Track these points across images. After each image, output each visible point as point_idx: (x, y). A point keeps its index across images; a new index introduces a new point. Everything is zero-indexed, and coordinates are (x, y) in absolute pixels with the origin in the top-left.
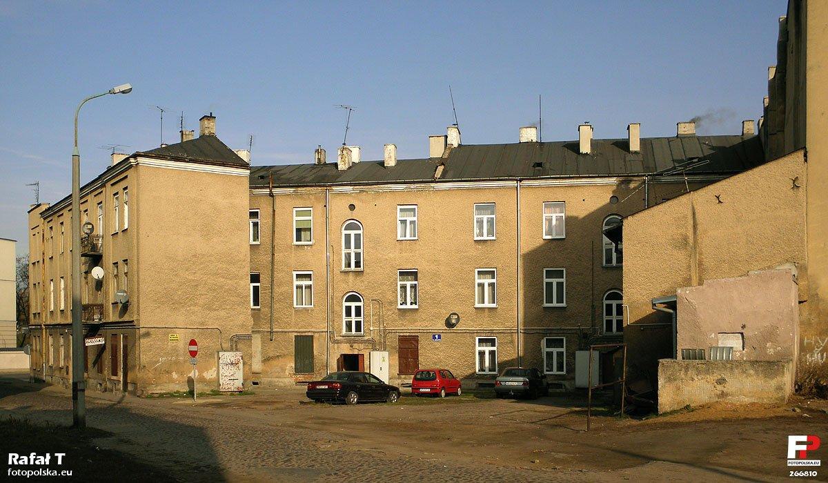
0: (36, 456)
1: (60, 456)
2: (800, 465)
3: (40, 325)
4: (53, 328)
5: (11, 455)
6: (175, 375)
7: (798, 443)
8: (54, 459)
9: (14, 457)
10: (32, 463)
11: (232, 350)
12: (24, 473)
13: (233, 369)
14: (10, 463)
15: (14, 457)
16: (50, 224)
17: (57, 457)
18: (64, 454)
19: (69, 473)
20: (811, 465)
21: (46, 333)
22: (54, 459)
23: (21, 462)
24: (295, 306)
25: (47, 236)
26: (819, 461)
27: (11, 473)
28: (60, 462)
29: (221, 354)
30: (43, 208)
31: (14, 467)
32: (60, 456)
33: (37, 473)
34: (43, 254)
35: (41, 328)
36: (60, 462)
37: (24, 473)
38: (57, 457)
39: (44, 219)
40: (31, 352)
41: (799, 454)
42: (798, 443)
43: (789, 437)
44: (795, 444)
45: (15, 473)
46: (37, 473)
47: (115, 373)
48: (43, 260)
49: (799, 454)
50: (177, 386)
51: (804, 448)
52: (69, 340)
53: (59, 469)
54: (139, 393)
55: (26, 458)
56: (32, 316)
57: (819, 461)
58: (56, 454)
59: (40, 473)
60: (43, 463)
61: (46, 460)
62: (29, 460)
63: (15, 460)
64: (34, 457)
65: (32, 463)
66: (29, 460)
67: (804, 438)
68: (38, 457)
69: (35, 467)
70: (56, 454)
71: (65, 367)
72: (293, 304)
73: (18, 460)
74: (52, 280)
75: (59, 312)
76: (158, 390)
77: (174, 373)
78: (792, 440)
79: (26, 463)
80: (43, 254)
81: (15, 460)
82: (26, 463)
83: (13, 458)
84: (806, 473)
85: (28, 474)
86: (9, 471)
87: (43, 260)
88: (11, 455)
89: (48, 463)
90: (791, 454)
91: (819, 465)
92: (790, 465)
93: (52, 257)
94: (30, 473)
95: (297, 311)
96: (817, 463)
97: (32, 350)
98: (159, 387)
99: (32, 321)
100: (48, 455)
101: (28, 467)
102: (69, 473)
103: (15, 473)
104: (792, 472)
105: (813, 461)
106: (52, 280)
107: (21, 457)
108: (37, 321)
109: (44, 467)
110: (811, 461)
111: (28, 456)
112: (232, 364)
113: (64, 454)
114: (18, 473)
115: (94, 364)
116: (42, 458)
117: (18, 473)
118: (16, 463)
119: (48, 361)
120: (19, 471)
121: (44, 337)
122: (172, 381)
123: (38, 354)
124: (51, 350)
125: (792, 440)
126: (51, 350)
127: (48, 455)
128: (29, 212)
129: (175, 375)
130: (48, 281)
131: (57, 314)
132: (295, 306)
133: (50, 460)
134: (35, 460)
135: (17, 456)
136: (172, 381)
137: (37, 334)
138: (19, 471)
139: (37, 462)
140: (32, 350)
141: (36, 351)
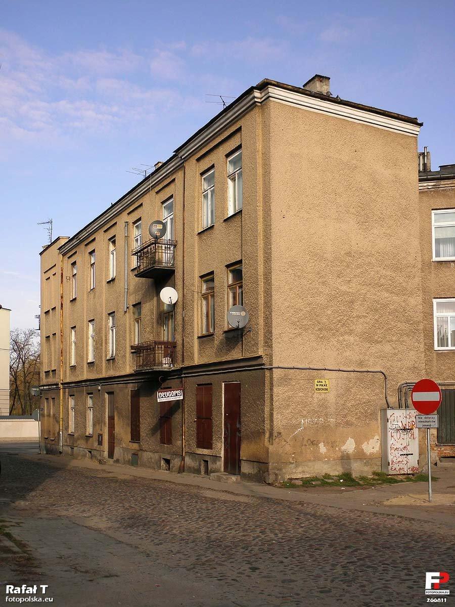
0: (27, 587)
1: (44, 587)
2: (435, 594)
3: (57, 384)
4: (76, 387)
5: (8, 587)
6: (323, 449)
7: (433, 578)
8: (39, 590)
9: (10, 588)
10: (23, 592)
11: (400, 407)
12: (18, 600)
13: (406, 437)
14: (7, 592)
15: (10, 588)
16: (72, 260)
17: (42, 588)
18: (47, 586)
19: (51, 600)
20: (443, 594)
21: (64, 393)
22: (39, 590)
23: (15, 592)
24: (436, 348)
25: (67, 273)
26: (449, 591)
27: (8, 599)
28: (44, 592)
29: (389, 412)
30: (62, 242)
31: (10, 595)
32: (44, 587)
33: (27, 600)
34: (62, 297)
35: (58, 389)
36: (44, 592)
37: (18, 600)
38: (42, 588)
39: (63, 255)
40: (41, 418)
41: (433, 585)
42: (433, 578)
43: (427, 573)
44: (431, 578)
45: (11, 600)
46: (27, 600)
47: (205, 441)
48: (62, 304)
49: (433, 585)
50: (326, 466)
51: (437, 581)
52: (104, 400)
53: (43, 596)
54: (271, 479)
55: (19, 589)
56: (43, 375)
57: (449, 591)
58: (41, 586)
59: (29, 600)
60: (31, 593)
61: (33, 590)
62: (21, 590)
63: (11, 590)
64: (25, 588)
65: (23, 592)
66: (21, 590)
67: (437, 574)
68: (28, 588)
69: (26, 595)
70: (41, 586)
71: (95, 437)
72: (433, 346)
73: (13, 590)
74: (74, 328)
75: (85, 365)
76: (299, 473)
77: (321, 445)
78: (429, 575)
79: (19, 592)
80: (62, 297)
81: (11, 590)
82: (19, 592)
83: (9, 589)
84: (439, 599)
85: (20, 600)
86: (7, 598)
87: (62, 304)
88: (8, 587)
89: (35, 592)
90: (428, 586)
91: (449, 594)
92: (427, 594)
93: (75, 299)
94: (22, 600)
95: (440, 354)
96: (447, 592)
97: (42, 415)
98: (300, 469)
99: (44, 381)
100: (35, 586)
101: (20, 595)
102: (51, 600)
103: (11, 600)
104: (429, 599)
105: (444, 591)
106: (74, 328)
107: (16, 588)
108: (51, 380)
109: (32, 595)
110: (442, 591)
111: (21, 587)
112: (405, 429)
113: (47, 586)
114: (13, 599)
115: (154, 431)
116: (31, 589)
117: (13, 599)
118: (12, 592)
119: (67, 428)
120: (14, 598)
121: (61, 398)
122: (318, 458)
123: (51, 419)
124: (72, 414)
125: (429, 575)
126: (72, 414)
127: (35, 586)
128: (41, 254)
129: (323, 449)
130: (68, 329)
131: (82, 367)
132: (436, 348)
133: (37, 590)
134: (26, 590)
135: (12, 587)
136: (318, 458)
137: (51, 395)
138: (14, 598)
139: (27, 592)
140: (42, 415)
141: (49, 416)
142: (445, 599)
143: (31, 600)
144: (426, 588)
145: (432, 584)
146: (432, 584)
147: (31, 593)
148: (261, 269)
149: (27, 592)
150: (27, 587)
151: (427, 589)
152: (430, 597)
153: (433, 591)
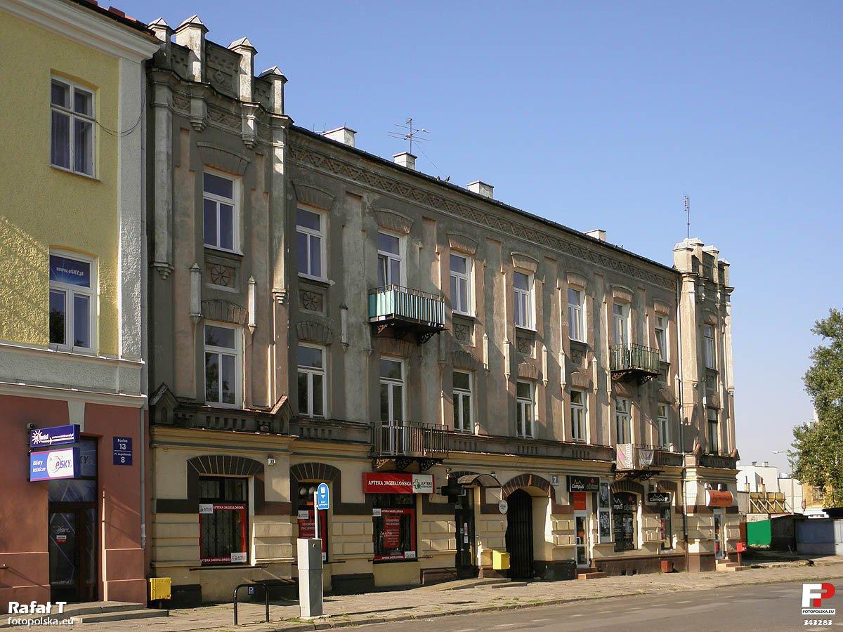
5: (11, 604)
7: (813, 592)
9: (14, 605)
14: (10, 611)
15: (14, 605)
20: (826, 614)
26: (834, 610)
42: (813, 592)
51: (818, 596)
57: (834, 610)
63: (15, 608)
64: (35, 606)
65: (32, 611)
68: (39, 606)
73: (18, 609)
81: (15, 608)
88: (11, 604)
90: (806, 603)
107: (22, 606)
116: (43, 606)
135: (17, 604)
142: (282, 302)
143: (43, 622)
144: (803, 606)
145: (481, 513)
146: (481, 513)
147: (43, 612)
148: (760, 565)
149: (21, 611)
150: (37, 604)
151: (804, 608)
152: (809, 618)
153: (813, 610)
